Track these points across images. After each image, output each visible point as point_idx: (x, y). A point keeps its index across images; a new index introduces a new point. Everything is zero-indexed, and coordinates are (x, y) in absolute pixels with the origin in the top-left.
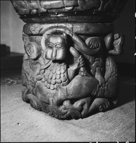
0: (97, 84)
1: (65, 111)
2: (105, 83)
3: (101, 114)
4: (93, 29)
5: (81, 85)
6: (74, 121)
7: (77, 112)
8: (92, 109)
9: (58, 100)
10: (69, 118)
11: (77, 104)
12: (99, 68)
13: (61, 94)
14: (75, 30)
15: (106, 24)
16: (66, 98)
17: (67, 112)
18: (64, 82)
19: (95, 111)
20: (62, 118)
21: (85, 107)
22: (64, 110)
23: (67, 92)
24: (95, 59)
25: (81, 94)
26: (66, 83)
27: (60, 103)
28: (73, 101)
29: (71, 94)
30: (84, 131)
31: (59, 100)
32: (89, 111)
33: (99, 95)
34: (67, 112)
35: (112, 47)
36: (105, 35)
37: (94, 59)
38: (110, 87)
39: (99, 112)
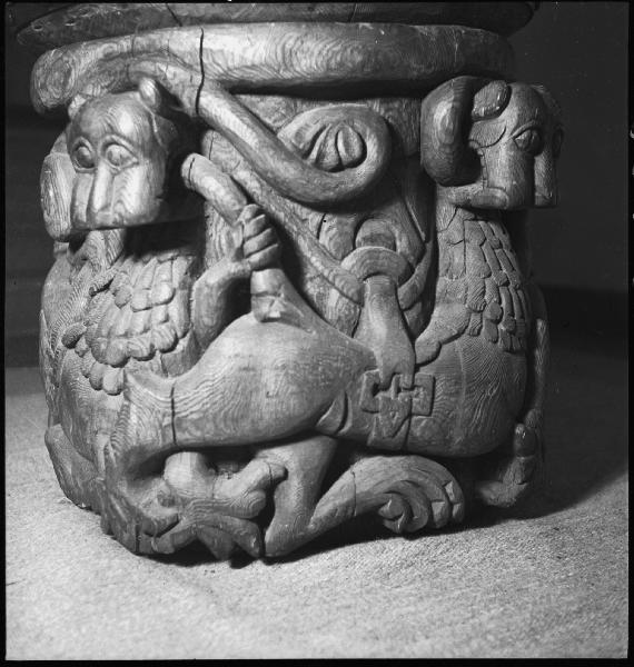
0: (359, 373)
1: (169, 512)
2: (417, 368)
3: (396, 548)
4: (320, 53)
5: (252, 373)
6: (220, 574)
7: (237, 522)
8: (332, 514)
9: (130, 452)
10: (191, 553)
11: (238, 486)
12: (384, 280)
13: (140, 418)
14: (214, 61)
15: (417, 27)
16: (170, 439)
17: (175, 522)
18: (163, 351)
19: (360, 526)
20: (156, 548)
21: (291, 496)
22: (163, 505)
23: (173, 407)
24: (357, 229)
25: (253, 421)
26: (179, 357)
27: (150, 465)
28: (220, 456)
29: (195, 416)
30: (226, 628)
31: (133, 449)
32: (311, 526)
33: (373, 433)
34: (175, 522)
35: (468, 164)
36: (419, 90)
37: (348, 229)
38: (451, 395)
39: (387, 534)
